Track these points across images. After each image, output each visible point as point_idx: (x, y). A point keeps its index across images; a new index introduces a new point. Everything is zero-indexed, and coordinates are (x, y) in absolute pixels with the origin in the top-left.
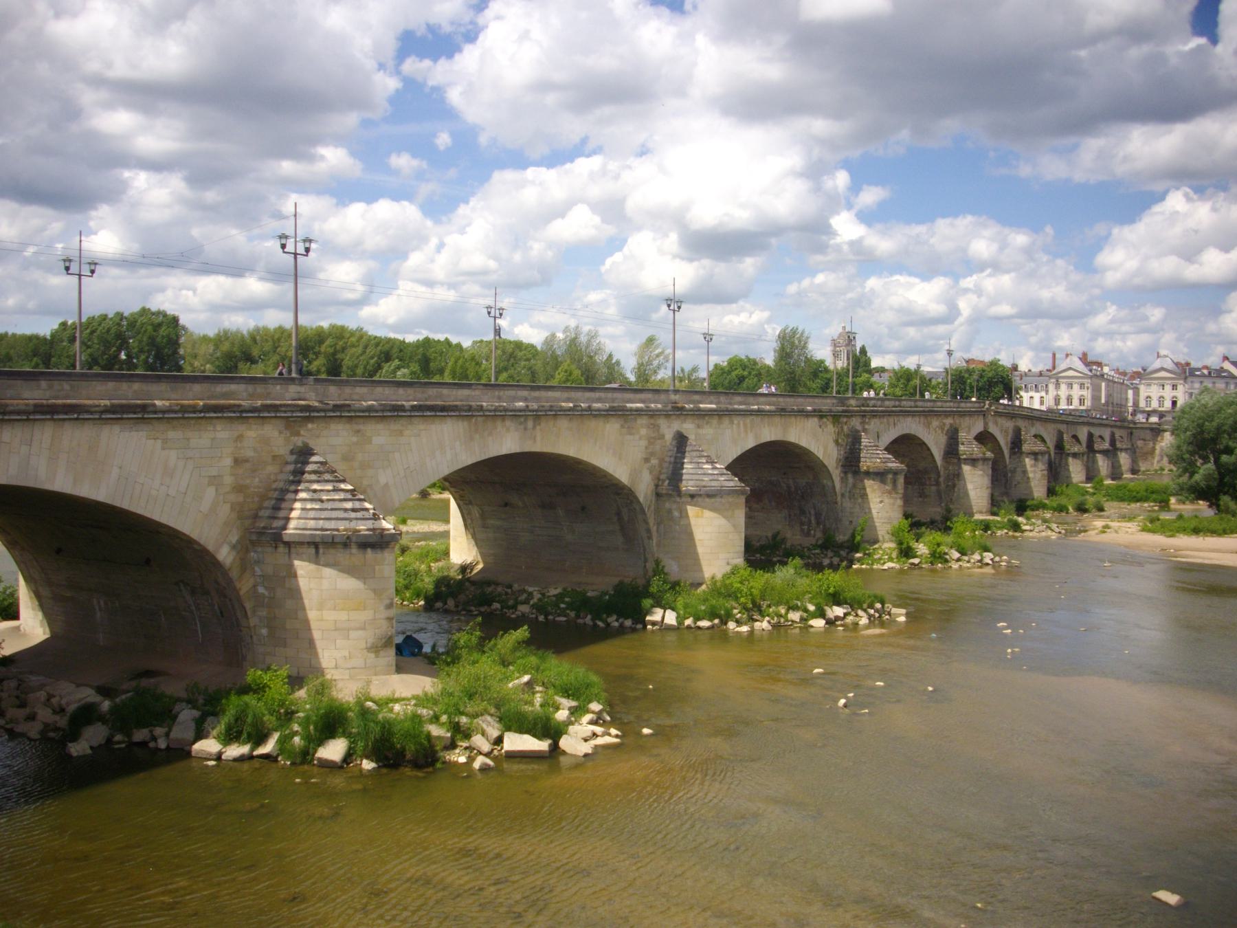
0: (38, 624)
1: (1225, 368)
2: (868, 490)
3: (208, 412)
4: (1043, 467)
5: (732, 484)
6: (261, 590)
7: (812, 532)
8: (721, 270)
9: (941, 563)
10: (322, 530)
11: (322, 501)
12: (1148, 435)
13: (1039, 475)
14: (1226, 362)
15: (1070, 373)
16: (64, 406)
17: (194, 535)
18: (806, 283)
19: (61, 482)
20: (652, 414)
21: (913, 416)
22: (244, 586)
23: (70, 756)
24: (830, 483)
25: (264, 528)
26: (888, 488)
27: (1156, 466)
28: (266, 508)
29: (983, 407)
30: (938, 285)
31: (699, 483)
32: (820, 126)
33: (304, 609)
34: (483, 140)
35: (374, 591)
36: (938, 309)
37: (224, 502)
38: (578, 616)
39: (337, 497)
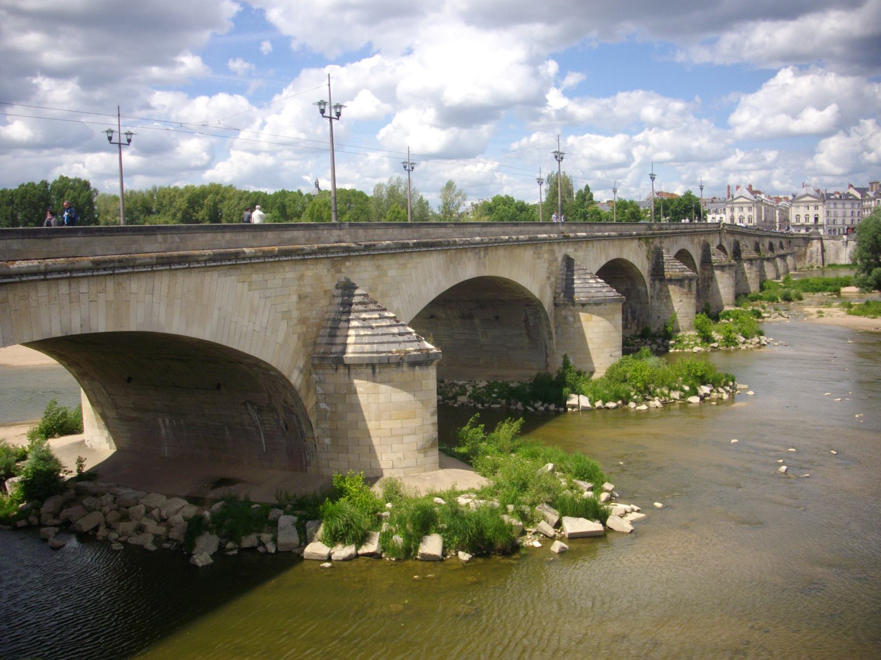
0: (104, 440)
1: (851, 193)
2: (671, 293)
3: (281, 256)
4: (756, 270)
5: (612, 294)
6: (323, 406)
7: (629, 326)
8: (465, 135)
9: (733, 346)
10: (378, 352)
11: (372, 328)
12: (801, 242)
13: (753, 275)
14: (851, 188)
15: (742, 200)
16: (179, 257)
17: (274, 364)
18: (524, 141)
19: (176, 326)
20: (549, 242)
21: (685, 235)
22: (310, 404)
23: (196, 566)
24: (643, 289)
25: (324, 353)
26: (685, 290)
27: (807, 265)
28: (322, 336)
29: (719, 227)
30: (620, 139)
31: (587, 294)
32: (538, 29)
33: (364, 420)
34: (294, 46)
35: (422, 401)
36: (618, 157)
37: (293, 334)
38: (509, 403)
39: (384, 324)
